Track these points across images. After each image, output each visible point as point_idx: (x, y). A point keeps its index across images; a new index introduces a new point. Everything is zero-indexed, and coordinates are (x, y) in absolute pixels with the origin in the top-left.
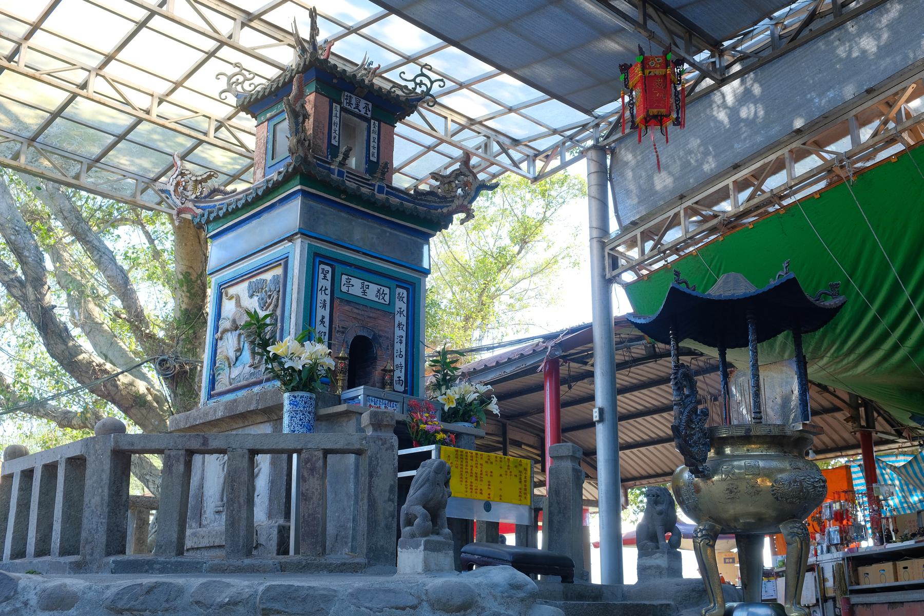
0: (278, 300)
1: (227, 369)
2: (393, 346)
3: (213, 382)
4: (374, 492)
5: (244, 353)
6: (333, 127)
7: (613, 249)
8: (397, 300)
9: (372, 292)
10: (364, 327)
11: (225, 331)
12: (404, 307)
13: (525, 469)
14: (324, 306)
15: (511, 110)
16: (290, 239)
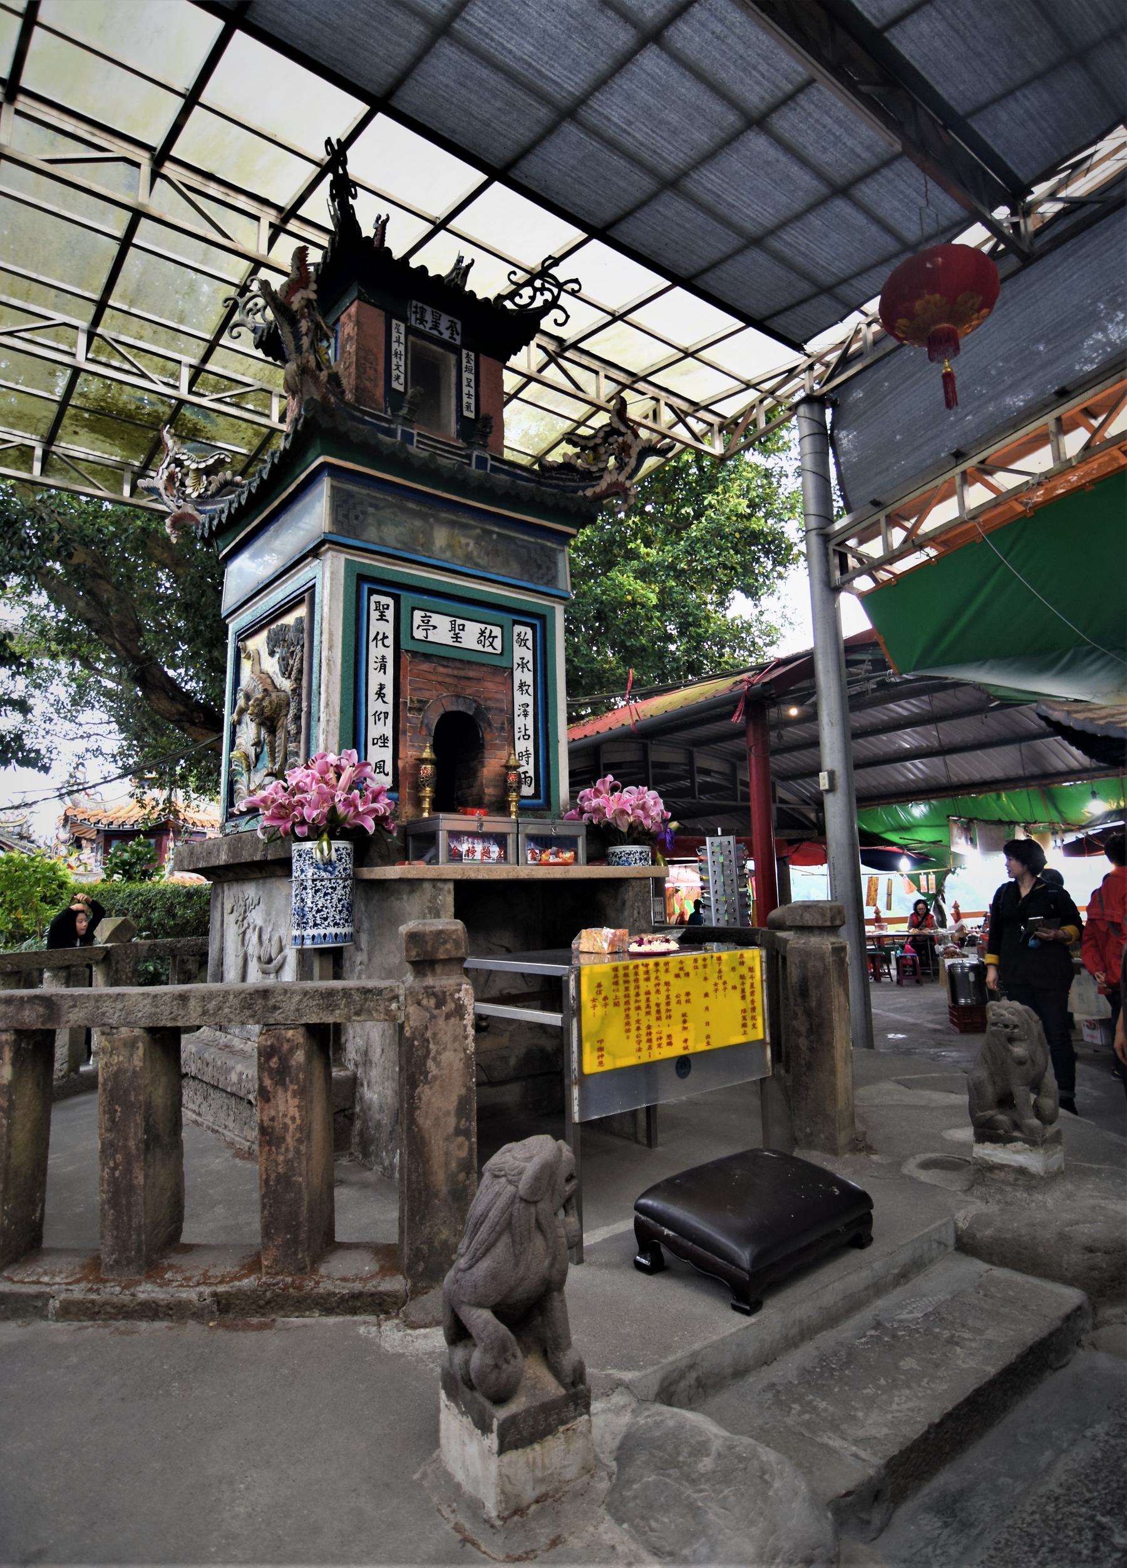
0: (302, 660)
1: (246, 775)
2: (512, 722)
4: (420, 1121)
6: (394, 361)
7: (839, 545)
8: (516, 645)
9: (471, 636)
10: (458, 696)
12: (528, 655)
13: (751, 970)
14: (383, 667)
15: (687, 354)
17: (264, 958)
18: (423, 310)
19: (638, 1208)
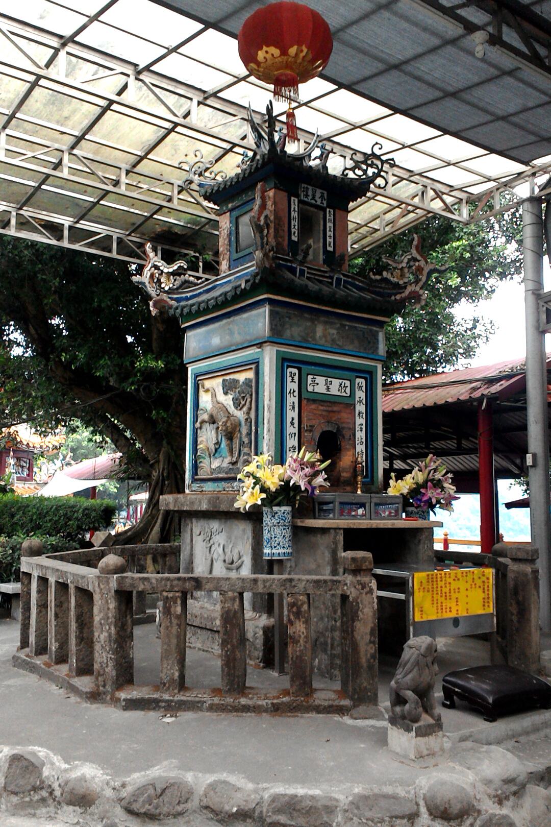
3: (195, 467)
4: (356, 636)
5: (222, 446)
6: (293, 223)
11: (203, 422)
12: (363, 395)
13: (488, 579)
14: (293, 408)
16: (260, 345)
17: (228, 560)
18: (307, 189)
19: (444, 680)
